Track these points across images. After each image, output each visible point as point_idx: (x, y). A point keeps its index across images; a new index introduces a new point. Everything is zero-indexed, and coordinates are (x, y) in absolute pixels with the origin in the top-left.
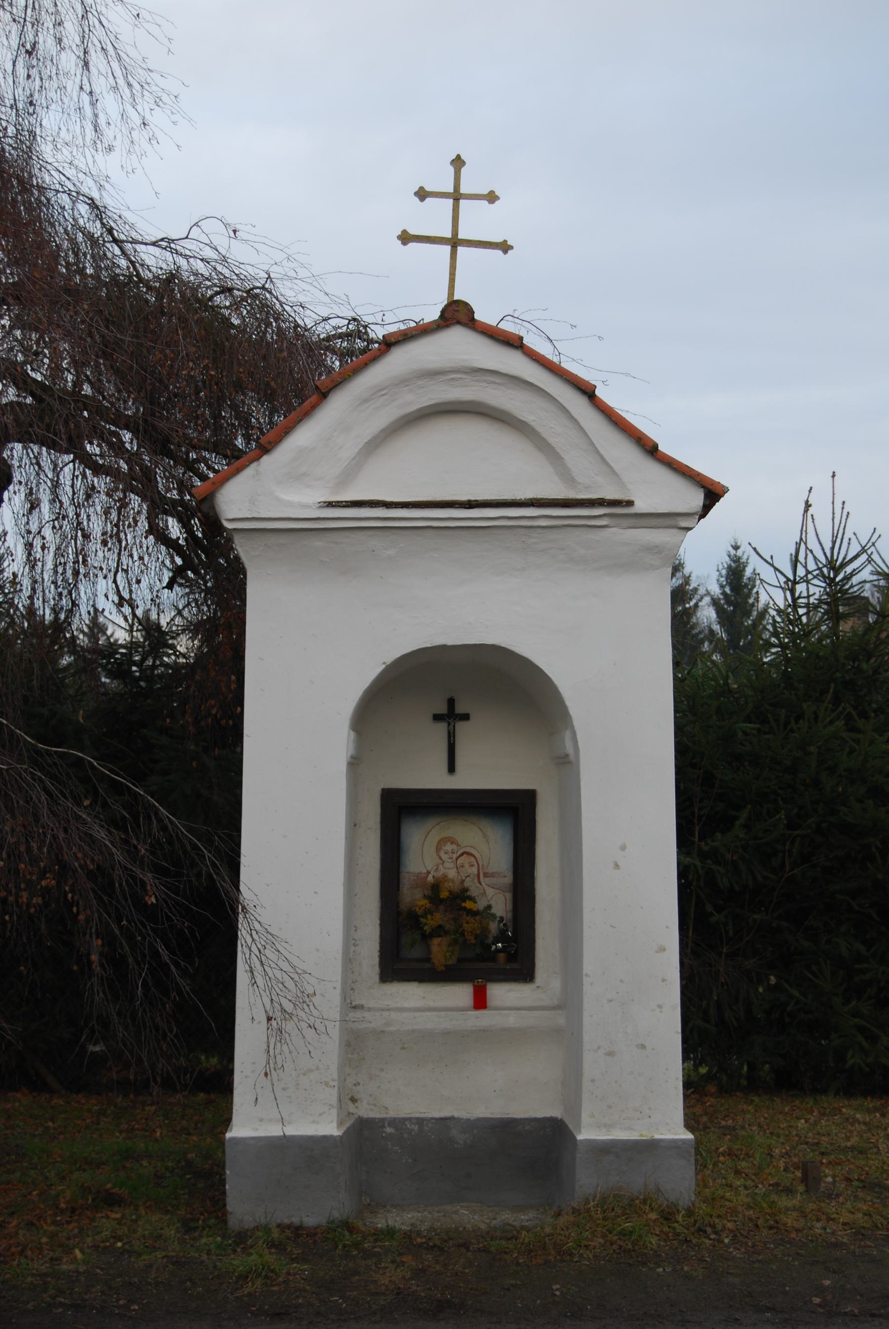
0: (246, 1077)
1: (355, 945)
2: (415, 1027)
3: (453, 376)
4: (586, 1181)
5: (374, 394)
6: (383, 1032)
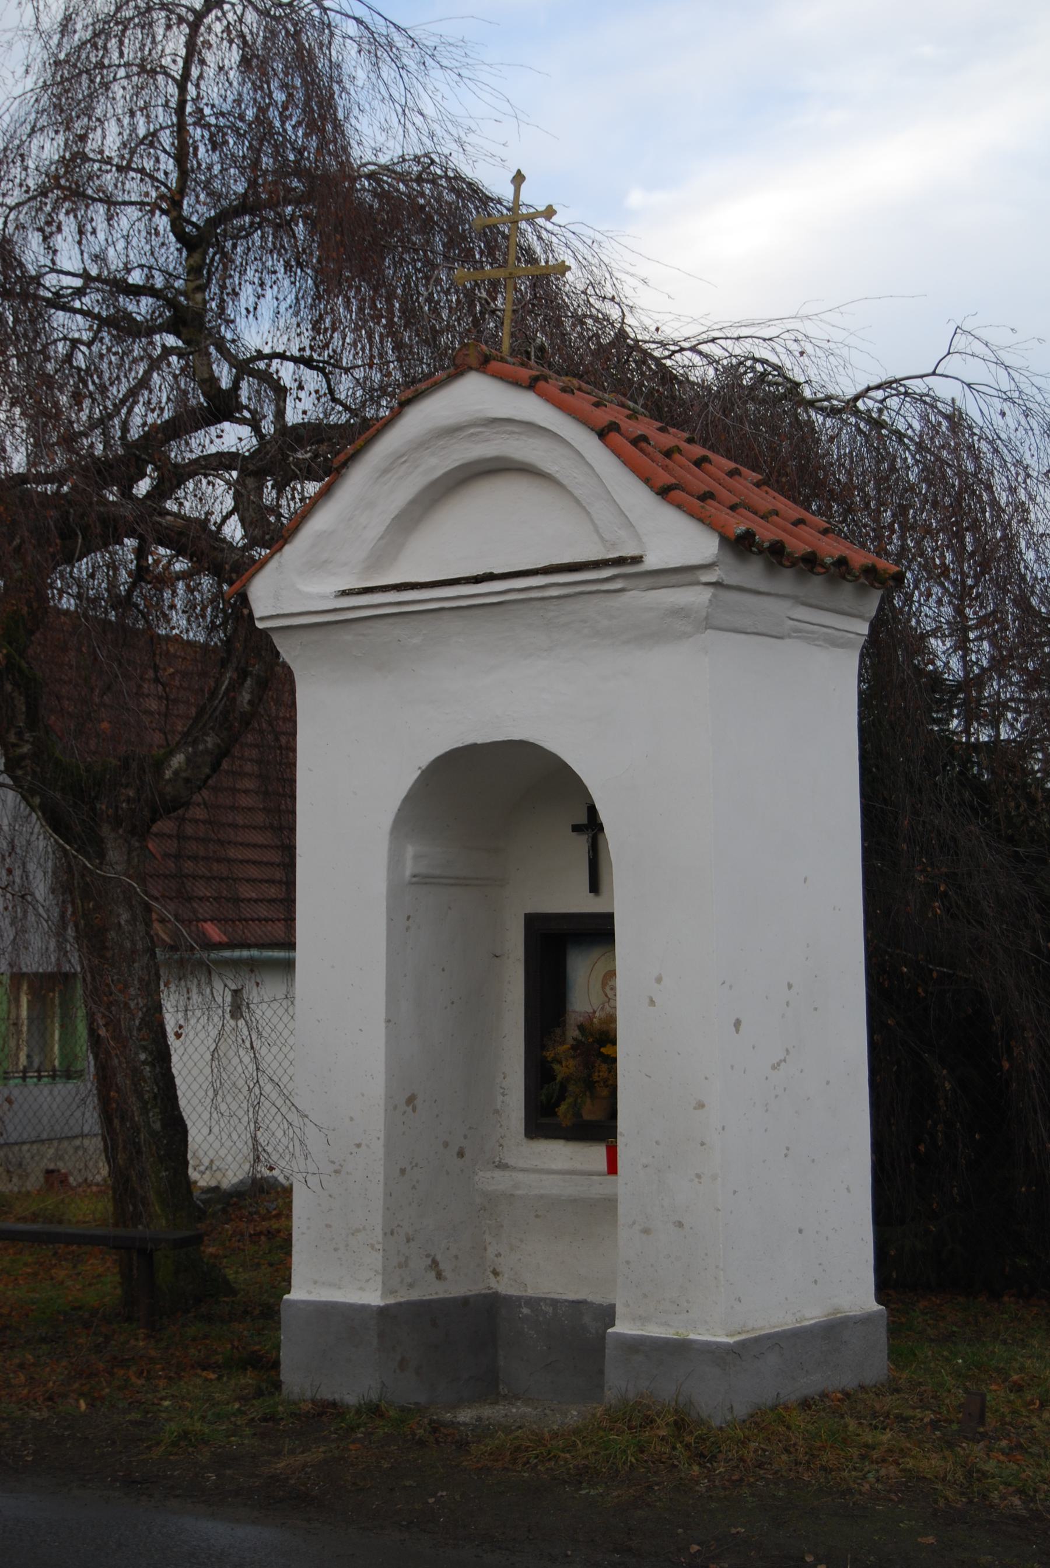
0: (303, 1233)
1: (503, 1095)
2: (542, 1192)
3: (472, 431)
4: (618, 1383)
5: (392, 463)
6: (512, 1195)
